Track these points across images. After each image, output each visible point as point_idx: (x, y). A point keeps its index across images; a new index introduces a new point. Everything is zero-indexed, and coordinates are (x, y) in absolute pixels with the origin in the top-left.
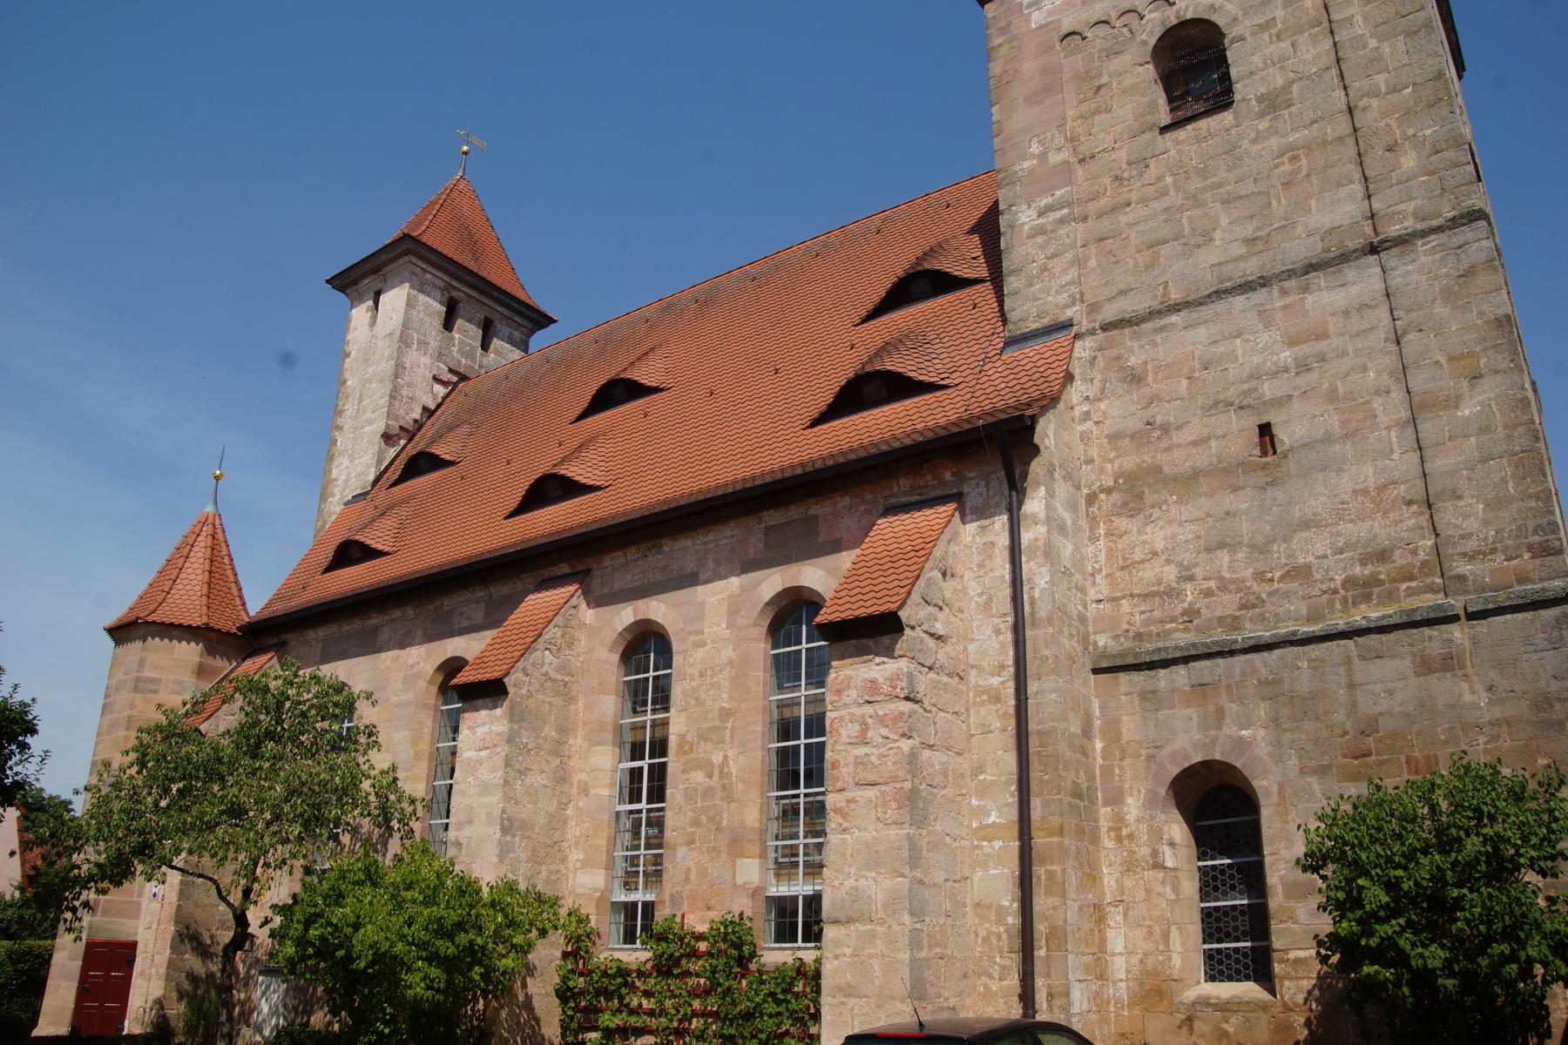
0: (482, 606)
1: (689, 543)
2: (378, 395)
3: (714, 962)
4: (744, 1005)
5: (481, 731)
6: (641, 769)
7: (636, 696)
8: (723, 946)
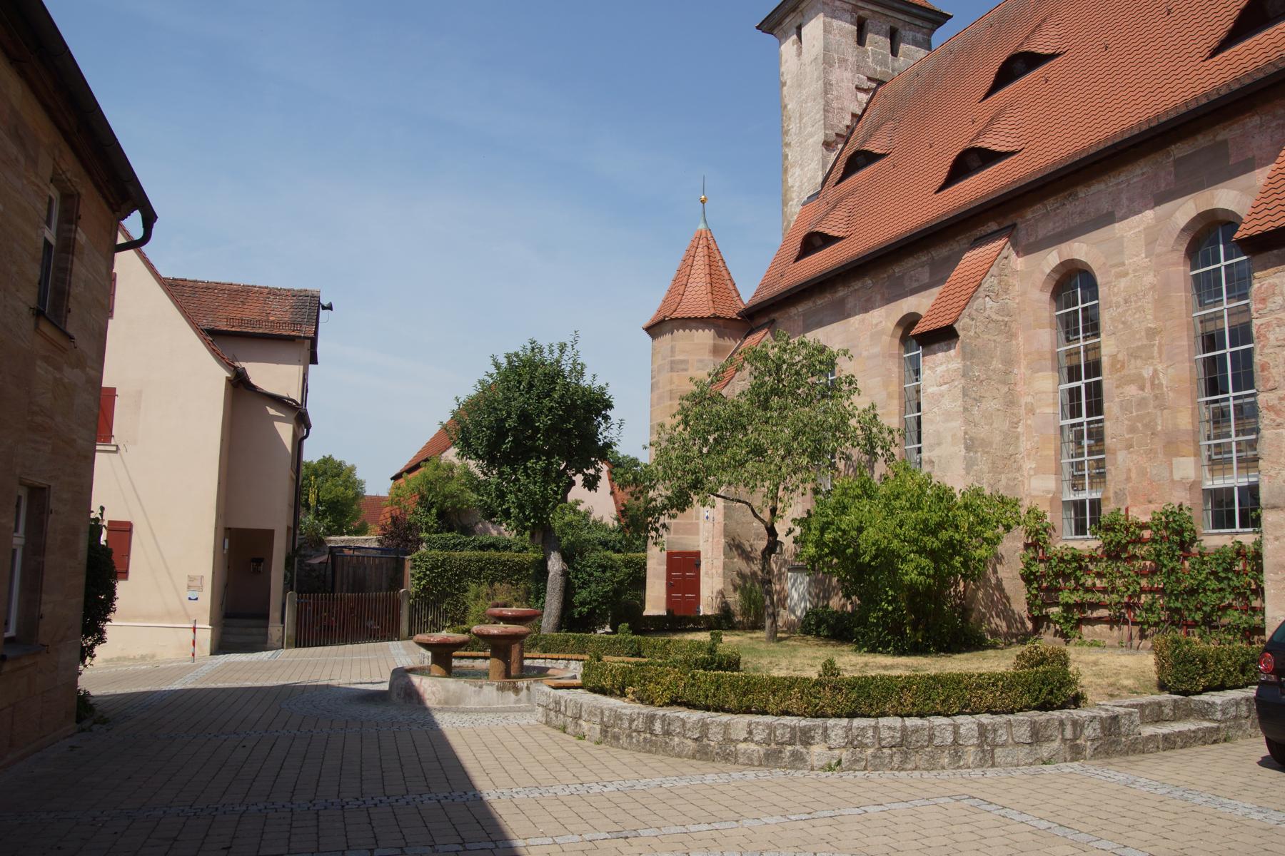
0: (927, 269)
1: (1102, 186)
2: (814, 111)
3: (1158, 547)
4: (1188, 583)
5: (940, 369)
6: (1079, 388)
7: (1068, 327)
8: (1165, 533)
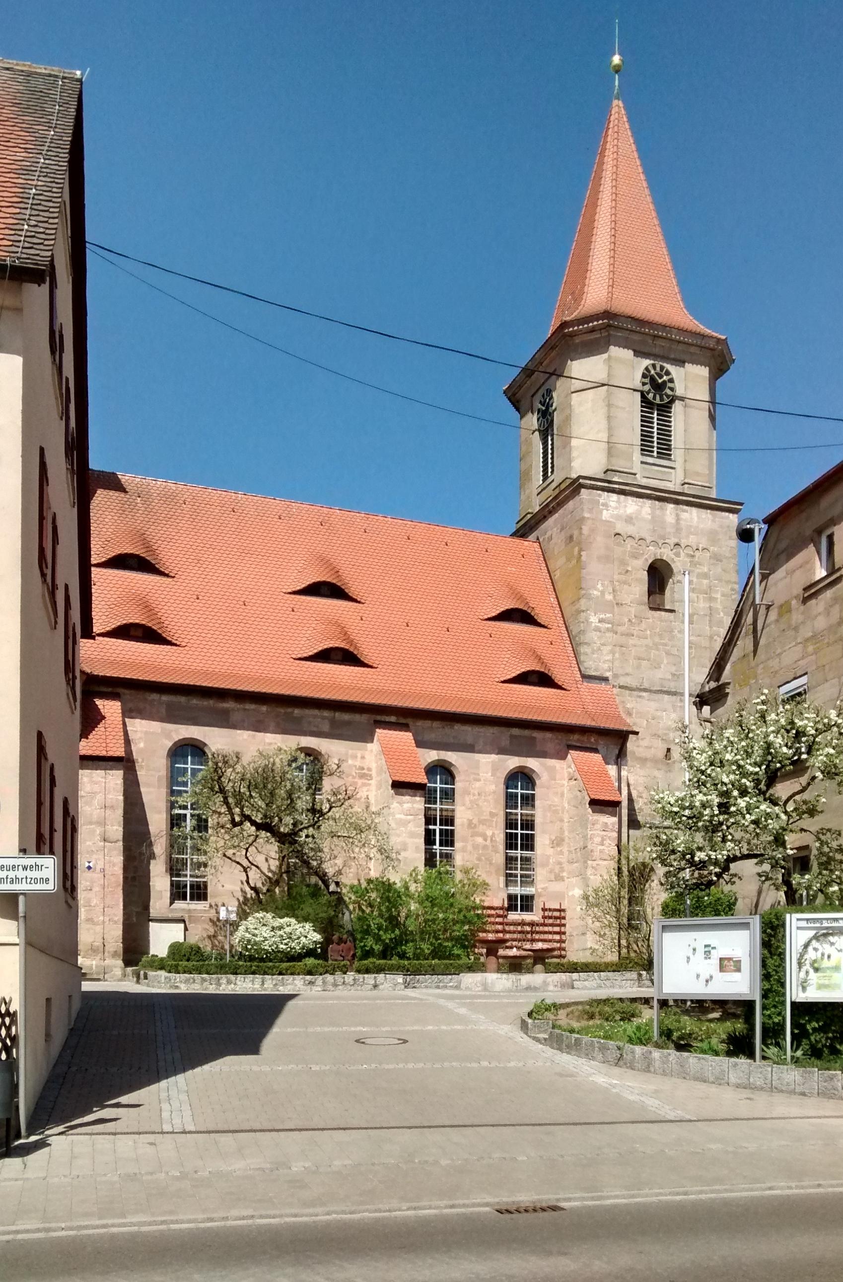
1: (470, 729)
5: (406, 806)
